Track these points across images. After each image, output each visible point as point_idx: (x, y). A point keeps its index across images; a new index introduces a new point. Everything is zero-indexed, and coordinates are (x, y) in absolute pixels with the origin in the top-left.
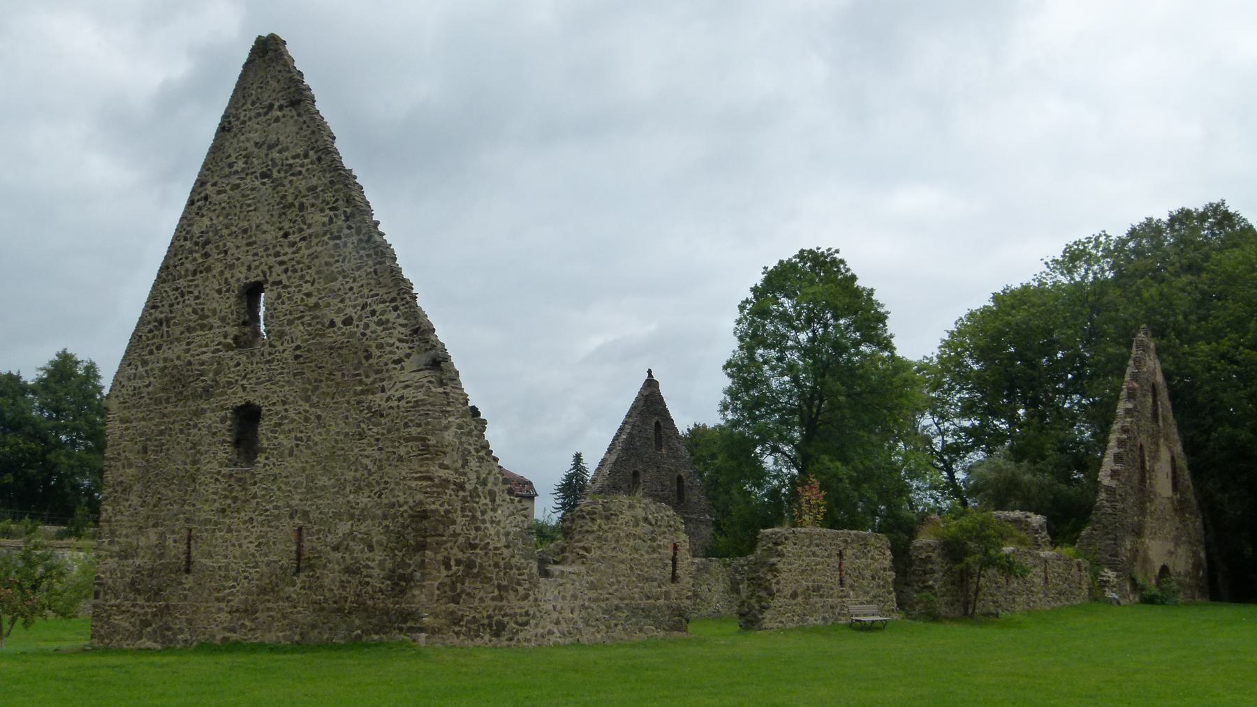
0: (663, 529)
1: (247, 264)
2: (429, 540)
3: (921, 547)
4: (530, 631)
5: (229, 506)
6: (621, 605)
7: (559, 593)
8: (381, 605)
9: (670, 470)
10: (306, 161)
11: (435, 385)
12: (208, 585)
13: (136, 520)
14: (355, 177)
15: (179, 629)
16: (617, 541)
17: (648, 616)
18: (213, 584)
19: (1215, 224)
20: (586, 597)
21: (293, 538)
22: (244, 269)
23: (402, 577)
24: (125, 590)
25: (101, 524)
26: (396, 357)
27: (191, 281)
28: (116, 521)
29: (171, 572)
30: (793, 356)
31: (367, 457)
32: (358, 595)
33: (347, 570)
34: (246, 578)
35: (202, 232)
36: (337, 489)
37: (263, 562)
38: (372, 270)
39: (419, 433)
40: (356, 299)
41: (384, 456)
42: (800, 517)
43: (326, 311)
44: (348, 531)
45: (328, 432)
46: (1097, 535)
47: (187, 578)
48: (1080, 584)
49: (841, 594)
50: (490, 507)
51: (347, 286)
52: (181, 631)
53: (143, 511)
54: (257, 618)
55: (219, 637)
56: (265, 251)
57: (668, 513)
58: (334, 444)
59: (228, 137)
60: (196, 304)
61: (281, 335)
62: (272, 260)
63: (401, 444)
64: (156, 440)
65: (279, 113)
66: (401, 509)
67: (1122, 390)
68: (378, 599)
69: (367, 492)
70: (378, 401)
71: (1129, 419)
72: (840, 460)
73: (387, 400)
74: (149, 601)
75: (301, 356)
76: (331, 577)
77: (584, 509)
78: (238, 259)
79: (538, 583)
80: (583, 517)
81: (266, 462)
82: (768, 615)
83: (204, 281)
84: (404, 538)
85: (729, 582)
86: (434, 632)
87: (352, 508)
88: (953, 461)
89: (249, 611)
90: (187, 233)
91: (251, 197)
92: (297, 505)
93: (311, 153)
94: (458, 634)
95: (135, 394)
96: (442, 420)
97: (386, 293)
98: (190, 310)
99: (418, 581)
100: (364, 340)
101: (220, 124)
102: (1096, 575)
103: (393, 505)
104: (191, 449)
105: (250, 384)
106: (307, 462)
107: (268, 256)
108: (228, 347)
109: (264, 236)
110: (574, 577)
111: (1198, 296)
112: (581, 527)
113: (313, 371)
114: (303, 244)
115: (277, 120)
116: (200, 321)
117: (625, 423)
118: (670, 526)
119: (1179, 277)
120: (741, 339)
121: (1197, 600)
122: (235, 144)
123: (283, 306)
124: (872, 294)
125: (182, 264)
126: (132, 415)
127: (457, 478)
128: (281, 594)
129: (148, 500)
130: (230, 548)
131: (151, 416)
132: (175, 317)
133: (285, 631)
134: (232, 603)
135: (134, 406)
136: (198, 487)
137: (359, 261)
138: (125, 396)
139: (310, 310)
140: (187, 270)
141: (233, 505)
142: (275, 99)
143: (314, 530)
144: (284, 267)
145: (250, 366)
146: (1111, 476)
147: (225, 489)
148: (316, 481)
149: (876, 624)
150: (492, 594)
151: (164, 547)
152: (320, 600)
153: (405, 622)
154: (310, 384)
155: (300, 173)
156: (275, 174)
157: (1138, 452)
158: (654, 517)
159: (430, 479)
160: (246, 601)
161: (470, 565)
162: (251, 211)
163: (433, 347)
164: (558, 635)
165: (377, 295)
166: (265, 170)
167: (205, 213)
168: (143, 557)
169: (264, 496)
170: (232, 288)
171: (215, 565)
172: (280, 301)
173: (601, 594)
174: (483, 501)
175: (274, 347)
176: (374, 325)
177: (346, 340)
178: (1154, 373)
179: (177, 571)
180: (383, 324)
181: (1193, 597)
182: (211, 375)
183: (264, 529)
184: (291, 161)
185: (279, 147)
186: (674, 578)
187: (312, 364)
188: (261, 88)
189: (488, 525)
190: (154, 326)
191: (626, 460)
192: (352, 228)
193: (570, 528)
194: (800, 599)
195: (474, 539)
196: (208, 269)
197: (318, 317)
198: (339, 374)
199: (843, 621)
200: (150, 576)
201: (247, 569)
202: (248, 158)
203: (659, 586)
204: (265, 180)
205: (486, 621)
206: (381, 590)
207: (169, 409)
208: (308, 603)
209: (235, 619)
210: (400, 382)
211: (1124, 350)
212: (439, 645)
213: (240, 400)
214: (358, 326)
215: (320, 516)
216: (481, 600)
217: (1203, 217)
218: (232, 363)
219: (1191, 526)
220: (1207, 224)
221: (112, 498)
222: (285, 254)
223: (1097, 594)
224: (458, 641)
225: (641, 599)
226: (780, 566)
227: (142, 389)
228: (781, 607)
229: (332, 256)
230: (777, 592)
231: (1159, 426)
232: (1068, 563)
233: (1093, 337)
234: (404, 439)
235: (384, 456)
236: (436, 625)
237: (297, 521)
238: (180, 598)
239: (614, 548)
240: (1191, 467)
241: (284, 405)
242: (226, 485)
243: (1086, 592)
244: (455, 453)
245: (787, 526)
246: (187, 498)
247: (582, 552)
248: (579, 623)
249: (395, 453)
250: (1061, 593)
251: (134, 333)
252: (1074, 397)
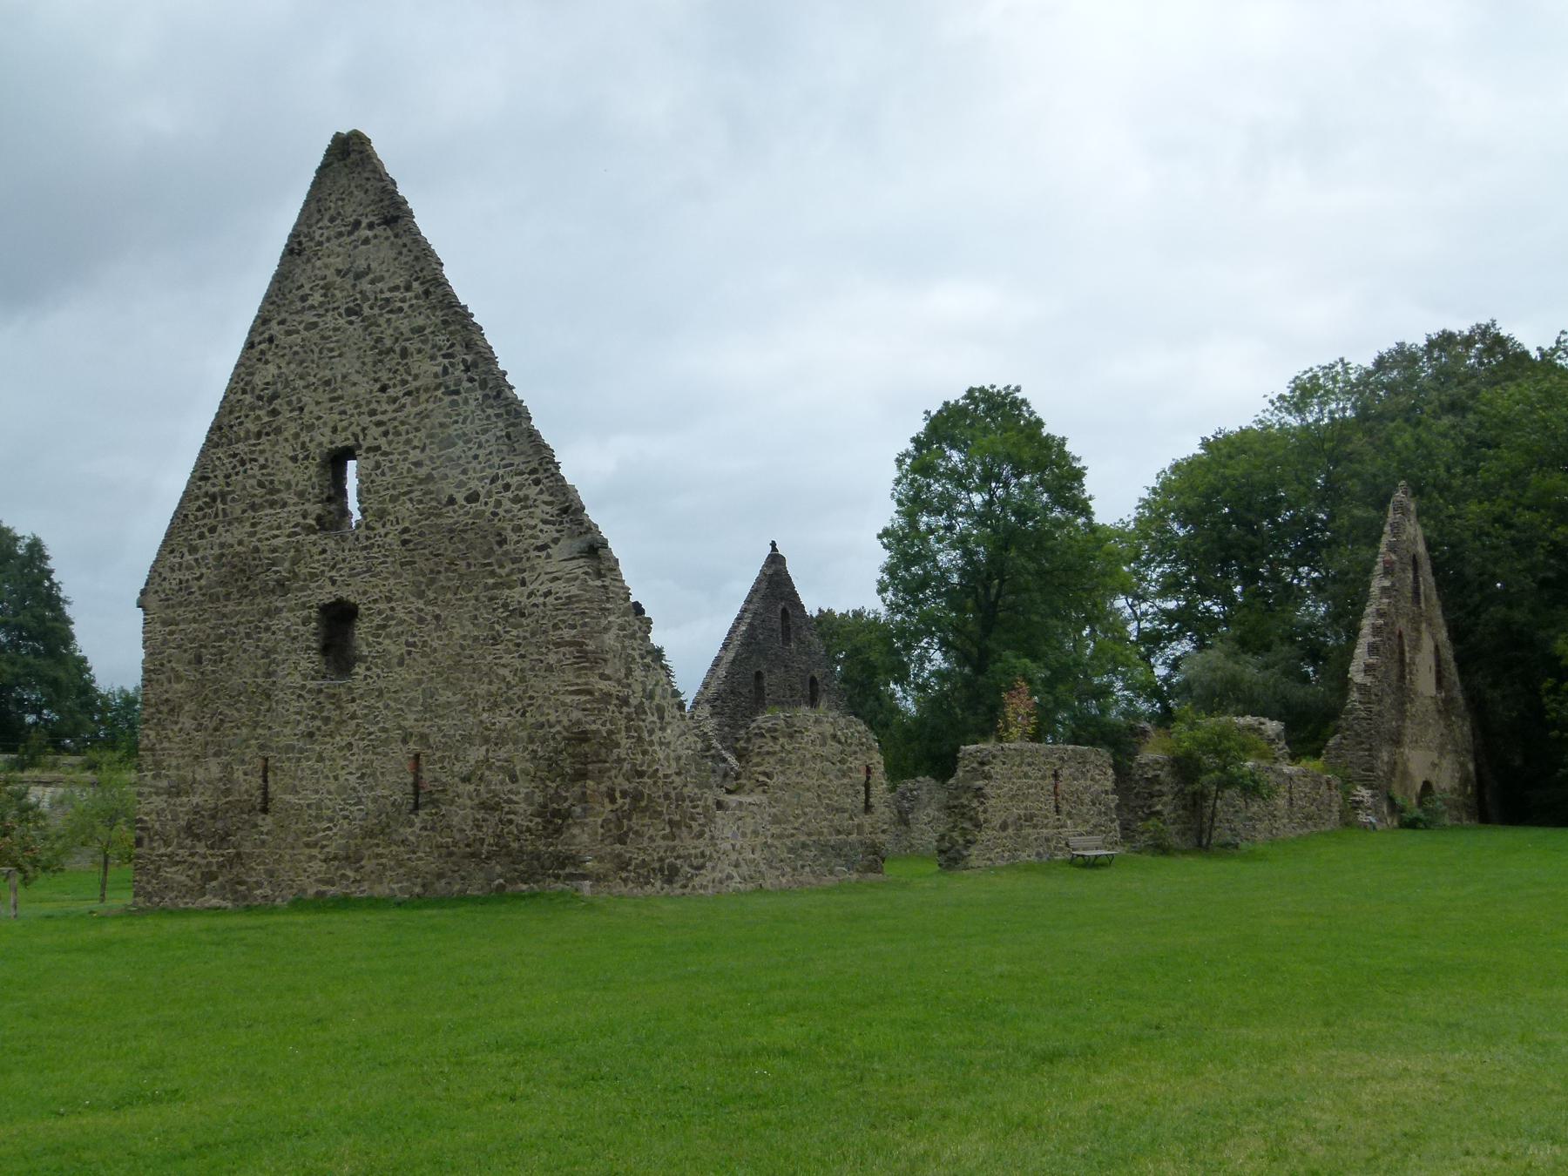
0: (853, 748)
1: (332, 424)
2: (590, 767)
3: (1147, 764)
4: (707, 876)
5: (319, 729)
6: (808, 842)
7: (738, 829)
8: (530, 848)
9: (801, 670)
10: (408, 295)
11: (593, 576)
12: (294, 827)
13: (189, 748)
14: (472, 315)
15: (256, 882)
16: (802, 764)
17: (839, 855)
18: (300, 826)
19: (1484, 351)
20: (769, 833)
21: (408, 768)
22: (327, 431)
23: (556, 813)
24: (178, 836)
25: (141, 753)
26: (540, 543)
27: (254, 445)
28: (163, 749)
29: (243, 812)
30: (961, 524)
31: (504, 666)
32: (499, 836)
33: (483, 806)
34: (346, 817)
35: (268, 383)
36: (465, 706)
37: (368, 797)
38: (504, 433)
39: (574, 636)
40: (482, 470)
41: (527, 665)
42: (1007, 730)
43: (443, 484)
44: (482, 758)
45: (451, 635)
46: (1347, 745)
47: (264, 819)
49: (1057, 823)
50: (659, 725)
51: (471, 453)
52: (259, 885)
53: (200, 737)
54: (362, 867)
55: (311, 892)
56: (356, 408)
57: (859, 728)
58: (459, 650)
59: (299, 262)
60: (263, 474)
61: (381, 515)
62: (366, 420)
63: (549, 650)
64: (213, 647)
65: (370, 234)
66: (553, 730)
67: (1376, 563)
68: (526, 840)
69: (505, 710)
70: (517, 596)
72: (1027, 656)
73: (529, 596)
74: (213, 849)
75: (410, 541)
76: (461, 814)
77: (763, 725)
78: (319, 418)
79: (715, 817)
80: (763, 736)
81: (368, 673)
82: (974, 851)
83: (274, 446)
84: (557, 765)
85: (896, 811)
86: (598, 879)
87: (487, 729)
88: (1151, 653)
89: (352, 859)
90: (247, 384)
91: (334, 339)
92: (412, 727)
93: (415, 285)
94: (625, 881)
95: (181, 589)
96: (602, 621)
97: (523, 463)
98: (254, 482)
99: (578, 817)
100: (496, 520)
101: (287, 246)
103: (542, 726)
104: (263, 658)
105: (341, 576)
106: (424, 673)
107: (360, 414)
108: (310, 530)
109: (353, 388)
110: (755, 809)
111: (1465, 443)
112: (760, 747)
113: (427, 560)
114: (408, 400)
115: (366, 241)
116: (268, 497)
117: (744, 611)
118: (862, 744)
119: (1440, 419)
120: (900, 503)
122: (309, 271)
123: (383, 478)
124: (1064, 445)
125: (241, 423)
126: (179, 615)
127: (619, 691)
128: (395, 836)
129: (206, 722)
130: (323, 781)
131: (206, 616)
132: (233, 492)
133: (401, 882)
134: (326, 850)
135: (180, 604)
136: (274, 705)
137: (485, 422)
138: (167, 591)
139: (420, 484)
140: (248, 432)
141: (323, 728)
142: (362, 215)
143: (436, 757)
144: (383, 429)
145: (340, 553)
146: (1365, 671)
147: (312, 708)
148: (436, 697)
150: (663, 832)
151: (230, 781)
152: (447, 842)
153: (563, 868)
154: (424, 576)
155: (401, 310)
156: (366, 311)
157: (1397, 641)
158: (843, 734)
159: (590, 693)
160: (347, 846)
161: (637, 797)
162: (334, 357)
163: (589, 530)
164: (738, 879)
165: (512, 465)
166: (351, 305)
167: (270, 359)
168: (203, 793)
169: (366, 715)
170: (312, 455)
171: (302, 802)
172: (379, 472)
173: (785, 829)
174: (650, 718)
175: (373, 529)
176: (509, 503)
177: (470, 521)
178: (1415, 542)
179: (250, 811)
180: (520, 501)
182: (287, 565)
183: (367, 757)
184: (387, 295)
185: (371, 276)
186: (868, 808)
187: (426, 551)
188: (343, 200)
189: (656, 748)
190: (205, 503)
191: (746, 658)
192: (475, 380)
193: (746, 749)
194: (1010, 831)
195: (641, 766)
196: (278, 431)
197: (432, 493)
198: (464, 563)
199: (1060, 857)
200: (213, 817)
201: (347, 807)
202: (329, 289)
203: (851, 819)
204: (353, 318)
205: (657, 865)
206: (529, 830)
207: (230, 608)
208: (431, 848)
209: (332, 868)
210: (546, 573)
211: (1373, 513)
212: (604, 895)
213: (328, 596)
214: (486, 504)
215: (443, 740)
216: (651, 839)
217: (1468, 341)
218: (314, 550)
219: (1458, 731)
220: (1473, 352)
221: (155, 721)
222: (384, 412)
223: (1348, 819)
224: (626, 890)
225: (831, 834)
226: (987, 790)
227: (191, 583)
228: (989, 840)
229: (448, 415)
230: (985, 822)
233: (1331, 494)
234: (554, 644)
235: (527, 665)
236: (601, 871)
237: (412, 746)
238: (255, 844)
239: (799, 773)
240: (1456, 658)
241: (389, 602)
242: (314, 703)
243: (1336, 816)
244: (616, 660)
245: (993, 741)
246: (261, 718)
247: (762, 778)
248: (762, 865)
249: (542, 662)
250: (1308, 817)
251: (176, 512)
252: (1301, 570)
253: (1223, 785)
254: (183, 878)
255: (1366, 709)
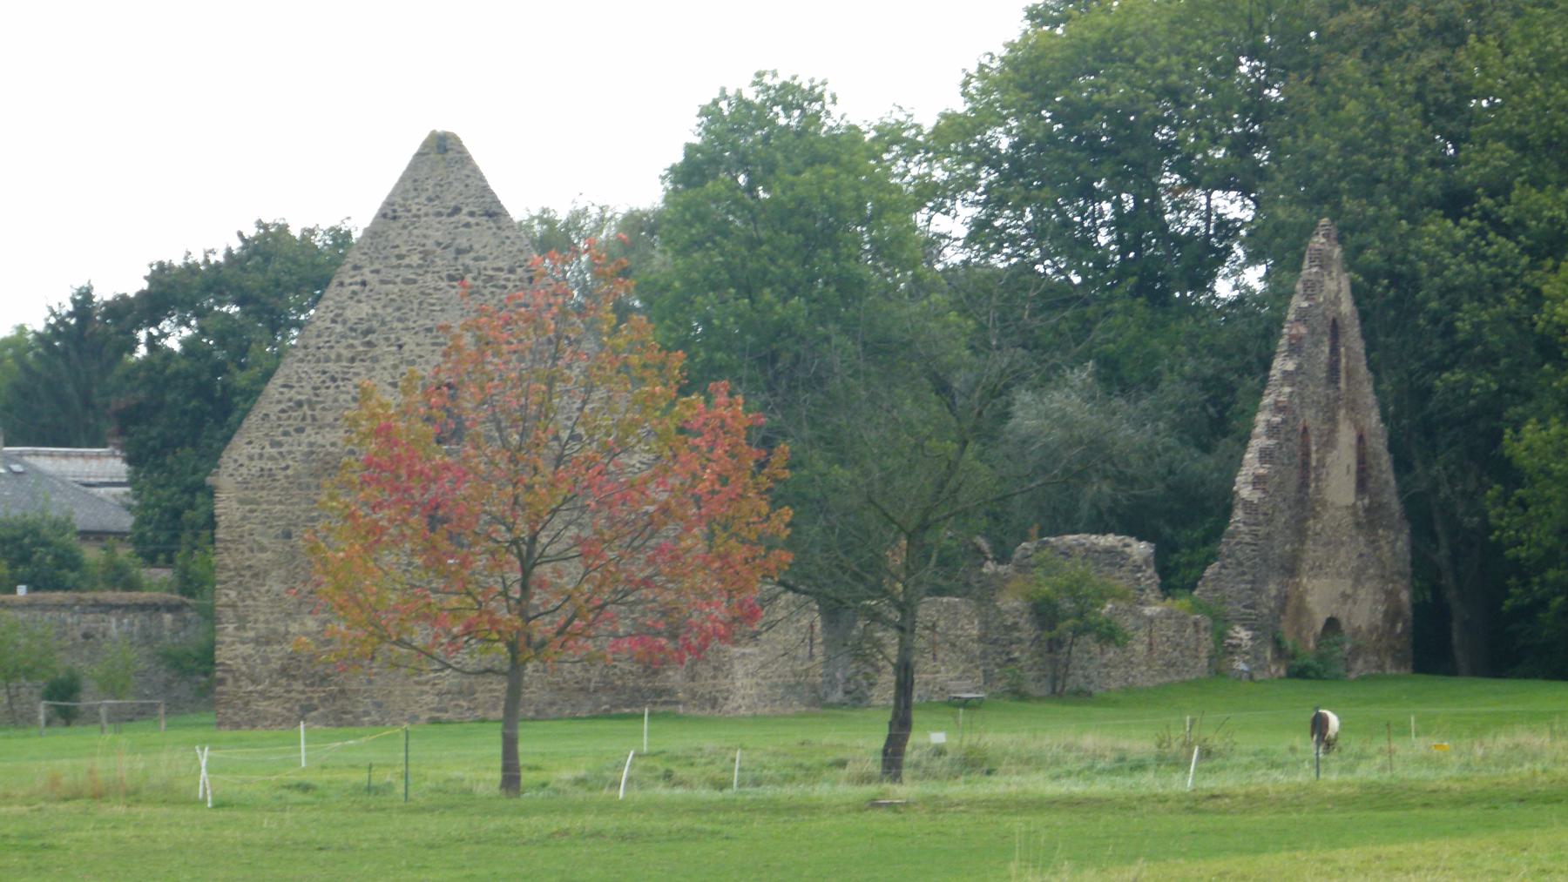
3: (1007, 612)
10: (512, 277)
46: (1228, 575)
48: (1196, 650)
71: (1287, 390)
78: (420, 357)
93: (519, 270)
98: (349, 397)
102: (1221, 636)
121: (1388, 672)
146: (1254, 484)
149: (970, 703)
153: (660, 697)
157: (1299, 441)
178: (1336, 301)
181: (1381, 667)
184: (491, 273)
200: (309, 661)
206: (631, 672)
214: (837, 557)
219: (1386, 548)
231: (1338, 389)
232: (1182, 623)
240: (1392, 447)
243: (1205, 662)
253: (1077, 632)
254: (279, 710)
255: (1250, 533)
